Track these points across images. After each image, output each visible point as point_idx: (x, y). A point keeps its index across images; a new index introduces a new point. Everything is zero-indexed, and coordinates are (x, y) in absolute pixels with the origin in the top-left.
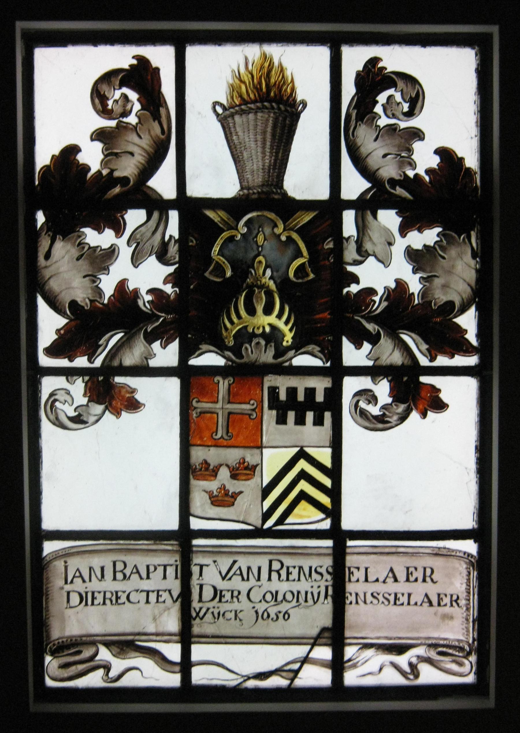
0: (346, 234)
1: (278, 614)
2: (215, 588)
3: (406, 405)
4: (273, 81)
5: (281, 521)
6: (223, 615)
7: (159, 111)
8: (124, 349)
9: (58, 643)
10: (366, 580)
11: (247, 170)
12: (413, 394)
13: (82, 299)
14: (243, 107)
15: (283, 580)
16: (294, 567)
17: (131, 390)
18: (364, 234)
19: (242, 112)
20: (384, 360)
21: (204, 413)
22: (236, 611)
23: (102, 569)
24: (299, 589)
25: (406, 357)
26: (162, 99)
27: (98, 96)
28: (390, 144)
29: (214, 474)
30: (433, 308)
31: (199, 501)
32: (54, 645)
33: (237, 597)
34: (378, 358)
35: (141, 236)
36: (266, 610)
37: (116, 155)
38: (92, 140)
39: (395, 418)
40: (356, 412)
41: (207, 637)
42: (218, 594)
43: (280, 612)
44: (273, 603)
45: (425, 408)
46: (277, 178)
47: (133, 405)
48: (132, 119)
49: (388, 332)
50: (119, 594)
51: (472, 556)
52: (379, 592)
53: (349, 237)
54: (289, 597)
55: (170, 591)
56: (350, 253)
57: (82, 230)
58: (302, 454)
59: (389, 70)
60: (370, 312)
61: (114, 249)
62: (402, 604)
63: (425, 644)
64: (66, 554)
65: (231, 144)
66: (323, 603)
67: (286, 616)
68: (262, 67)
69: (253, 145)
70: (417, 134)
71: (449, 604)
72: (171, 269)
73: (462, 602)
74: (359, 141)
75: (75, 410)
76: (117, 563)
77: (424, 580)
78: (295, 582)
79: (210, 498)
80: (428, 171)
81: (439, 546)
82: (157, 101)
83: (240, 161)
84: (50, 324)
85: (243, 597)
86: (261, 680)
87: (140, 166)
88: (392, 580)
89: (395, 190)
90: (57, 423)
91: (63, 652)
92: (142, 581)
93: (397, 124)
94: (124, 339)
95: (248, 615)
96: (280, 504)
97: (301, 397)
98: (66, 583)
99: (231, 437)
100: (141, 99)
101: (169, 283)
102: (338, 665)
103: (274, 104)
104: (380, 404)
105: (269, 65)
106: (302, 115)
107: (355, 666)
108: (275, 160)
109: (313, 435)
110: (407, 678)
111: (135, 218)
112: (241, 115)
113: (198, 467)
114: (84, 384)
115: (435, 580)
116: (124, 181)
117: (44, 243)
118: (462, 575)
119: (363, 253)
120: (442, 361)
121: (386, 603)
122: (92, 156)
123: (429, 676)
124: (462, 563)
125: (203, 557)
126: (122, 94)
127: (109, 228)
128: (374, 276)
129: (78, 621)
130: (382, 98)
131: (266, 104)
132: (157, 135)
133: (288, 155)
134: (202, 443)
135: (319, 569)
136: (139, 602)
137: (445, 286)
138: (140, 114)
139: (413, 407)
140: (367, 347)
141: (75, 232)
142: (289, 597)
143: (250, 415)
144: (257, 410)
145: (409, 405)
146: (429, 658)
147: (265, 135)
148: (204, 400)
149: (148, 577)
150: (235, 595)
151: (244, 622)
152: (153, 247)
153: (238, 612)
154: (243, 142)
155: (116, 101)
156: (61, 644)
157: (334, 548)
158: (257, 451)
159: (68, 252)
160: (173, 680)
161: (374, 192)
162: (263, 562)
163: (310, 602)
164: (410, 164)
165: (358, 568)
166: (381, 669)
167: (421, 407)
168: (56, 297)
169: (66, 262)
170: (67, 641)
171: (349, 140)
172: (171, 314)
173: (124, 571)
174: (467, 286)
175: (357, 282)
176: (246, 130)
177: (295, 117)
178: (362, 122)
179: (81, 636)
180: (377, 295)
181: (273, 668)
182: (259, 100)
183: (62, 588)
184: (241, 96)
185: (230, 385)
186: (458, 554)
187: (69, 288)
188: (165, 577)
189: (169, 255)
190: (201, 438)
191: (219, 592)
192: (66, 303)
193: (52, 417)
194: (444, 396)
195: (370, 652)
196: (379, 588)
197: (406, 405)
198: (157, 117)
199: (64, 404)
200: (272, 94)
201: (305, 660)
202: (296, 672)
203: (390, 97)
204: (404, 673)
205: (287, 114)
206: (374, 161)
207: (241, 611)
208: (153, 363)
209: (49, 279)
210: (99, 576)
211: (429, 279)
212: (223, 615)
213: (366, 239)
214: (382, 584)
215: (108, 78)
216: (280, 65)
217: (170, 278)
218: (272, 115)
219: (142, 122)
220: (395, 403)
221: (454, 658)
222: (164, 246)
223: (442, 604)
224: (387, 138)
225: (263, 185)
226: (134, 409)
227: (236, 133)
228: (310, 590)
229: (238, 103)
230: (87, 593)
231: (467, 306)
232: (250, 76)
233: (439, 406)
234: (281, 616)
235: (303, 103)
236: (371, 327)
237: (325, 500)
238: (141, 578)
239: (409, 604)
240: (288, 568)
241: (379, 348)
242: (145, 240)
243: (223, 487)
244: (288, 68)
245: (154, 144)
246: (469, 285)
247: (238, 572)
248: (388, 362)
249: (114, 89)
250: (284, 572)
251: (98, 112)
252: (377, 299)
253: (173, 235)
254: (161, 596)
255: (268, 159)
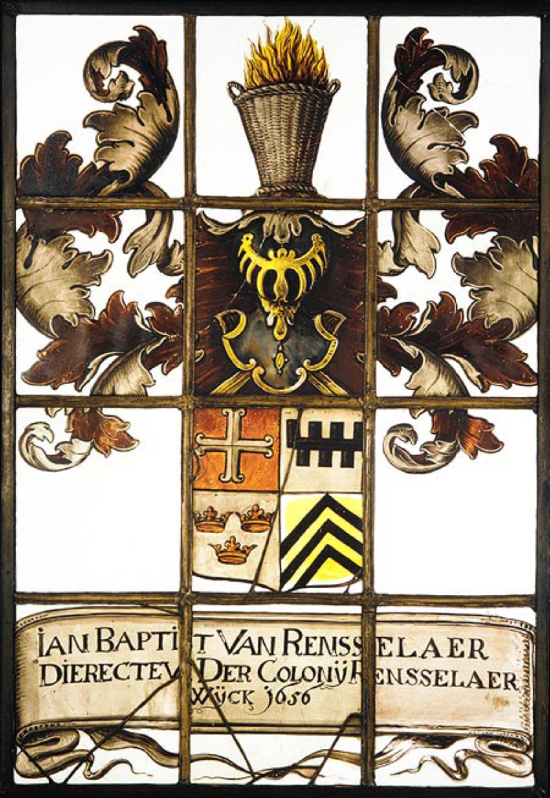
0: (381, 240)
1: (296, 695)
2: (218, 662)
3: (452, 444)
4: (300, 57)
5: (303, 582)
6: (230, 696)
7: (165, 92)
8: (118, 374)
9: (31, 729)
10: (401, 654)
11: (269, 163)
12: (459, 429)
13: (68, 315)
14: (264, 88)
15: (301, 654)
16: (315, 638)
17: (122, 424)
18: (402, 239)
19: (263, 95)
20: (426, 388)
21: (210, 451)
22: (245, 692)
23: (85, 637)
24: (321, 665)
25: (453, 387)
26: (168, 79)
27: (92, 75)
28: (438, 132)
29: (221, 524)
30: (486, 326)
31: (205, 559)
32: (25, 732)
33: (246, 675)
34: (420, 387)
35: (140, 240)
36: (281, 691)
37: (113, 144)
38: (85, 126)
39: (439, 457)
40: (391, 452)
41: (209, 725)
42: (223, 670)
43: (298, 693)
44: (289, 682)
45: (475, 447)
46: (304, 173)
47: (125, 442)
48: (133, 102)
49: (431, 355)
50: (105, 668)
51: (531, 627)
52: (416, 669)
53: (385, 243)
54: (309, 674)
55: (166, 664)
56: (387, 262)
57: (70, 232)
58: (328, 502)
59: (436, 43)
60: (410, 332)
61: (107, 256)
62: (446, 685)
63: (474, 735)
64: (42, 620)
65: (251, 132)
66: (350, 683)
67: (306, 699)
68: (287, 41)
69: (276, 133)
70: (469, 120)
71: (503, 686)
72: (175, 280)
73: (519, 683)
74: (400, 129)
75: (56, 449)
76: (103, 631)
77: (472, 656)
78: (316, 657)
79: (217, 554)
80: (483, 165)
81: (490, 614)
82: (163, 81)
83: (260, 153)
84: (29, 344)
85: (253, 675)
86: (275, 778)
87: (142, 158)
88: (433, 654)
89: (444, 188)
90: (34, 462)
91: (36, 740)
92: (133, 652)
93: (447, 108)
94: (119, 362)
95: (259, 697)
96: (301, 562)
97: (326, 434)
98: (41, 655)
99: (242, 480)
100: (142, 79)
101: (172, 296)
102: (368, 760)
103: (301, 85)
104: (421, 441)
105: (296, 38)
106: (335, 98)
107: (387, 762)
108: (303, 152)
109: (340, 480)
110: (454, 778)
111: (132, 219)
112: (262, 97)
113: (202, 516)
114: (66, 417)
115: (485, 656)
116: (124, 174)
117: (25, 247)
118: (519, 649)
119: (401, 262)
120: (496, 391)
121: (426, 682)
122: (84, 146)
123: (480, 776)
124: (519, 635)
125: (206, 626)
126: (121, 72)
127: (101, 231)
128: (415, 289)
129: (54, 701)
130: (428, 77)
131: (291, 85)
132: (162, 121)
133: (318, 146)
134: (208, 487)
135: (345, 641)
136: (128, 678)
137: (500, 301)
138: (143, 96)
139: (461, 446)
140: (405, 373)
141: (62, 234)
142: (309, 674)
143: (265, 454)
144: (273, 448)
145: (457, 443)
146: (480, 752)
147: (290, 122)
148: (211, 436)
149: (140, 648)
150: (244, 672)
151: (254, 705)
152: (153, 253)
153: (247, 693)
154: (264, 130)
155: (113, 81)
156: (33, 730)
157: (374, 622)
158: (274, 497)
159: (52, 258)
160: (169, 776)
161: (418, 190)
162: (278, 631)
163: (335, 681)
164: (462, 157)
165: (390, 639)
166: (420, 766)
167: (470, 445)
168: (37, 311)
169: (50, 271)
170: (41, 726)
171: (388, 128)
172: (175, 334)
173: (111, 640)
174: (527, 300)
175: (395, 296)
176: (268, 116)
177: (327, 100)
178: (404, 106)
179: (59, 721)
180: (418, 311)
181: (290, 764)
182: (283, 80)
183: (36, 661)
184: (262, 76)
185: (241, 417)
186: (513, 624)
187: (54, 301)
188: (160, 648)
189: (173, 264)
190: (207, 481)
191: (224, 669)
192: (49, 318)
193: (28, 456)
194: (497, 432)
195: (407, 744)
196: (417, 664)
197: (452, 444)
198: (161, 99)
199: (42, 441)
200: (299, 73)
201: (331, 754)
202: (318, 769)
203: (437, 76)
204: (449, 772)
205: (318, 97)
206: (418, 153)
207: (251, 692)
208: (152, 392)
209: (30, 290)
210: (82, 647)
211: (481, 293)
212: (230, 696)
213: (406, 245)
214: (421, 659)
215: (103, 52)
216: (309, 37)
217: (173, 290)
218: (299, 97)
219: (144, 106)
220: (439, 441)
221: (510, 753)
222: (167, 253)
223: (495, 685)
224: (433, 125)
225: (288, 182)
226: (126, 447)
227: (257, 119)
228: (334, 666)
229: (258, 84)
230: (66, 667)
231: (527, 325)
232: (272, 51)
233: (493, 444)
234: (299, 698)
235: (336, 84)
236: (411, 350)
237: (356, 558)
238: (132, 648)
239: (454, 685)
240: (307, 639)
241: (419, 374)
242: (144, 245)
243: (233, 540)
244: (318, 41)
245: (159, 133)
246: (530, 300)
247: (248, 644)
248: (432, 392)
249: (112, 66)
250: (302, 644)
251: (91, 92)
252: (418, 316)
253: (178, 239)
254: (156, 670)
255: (293, 151)
